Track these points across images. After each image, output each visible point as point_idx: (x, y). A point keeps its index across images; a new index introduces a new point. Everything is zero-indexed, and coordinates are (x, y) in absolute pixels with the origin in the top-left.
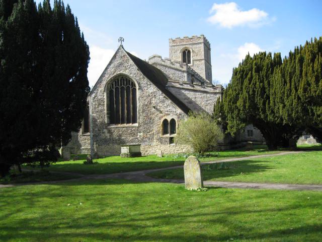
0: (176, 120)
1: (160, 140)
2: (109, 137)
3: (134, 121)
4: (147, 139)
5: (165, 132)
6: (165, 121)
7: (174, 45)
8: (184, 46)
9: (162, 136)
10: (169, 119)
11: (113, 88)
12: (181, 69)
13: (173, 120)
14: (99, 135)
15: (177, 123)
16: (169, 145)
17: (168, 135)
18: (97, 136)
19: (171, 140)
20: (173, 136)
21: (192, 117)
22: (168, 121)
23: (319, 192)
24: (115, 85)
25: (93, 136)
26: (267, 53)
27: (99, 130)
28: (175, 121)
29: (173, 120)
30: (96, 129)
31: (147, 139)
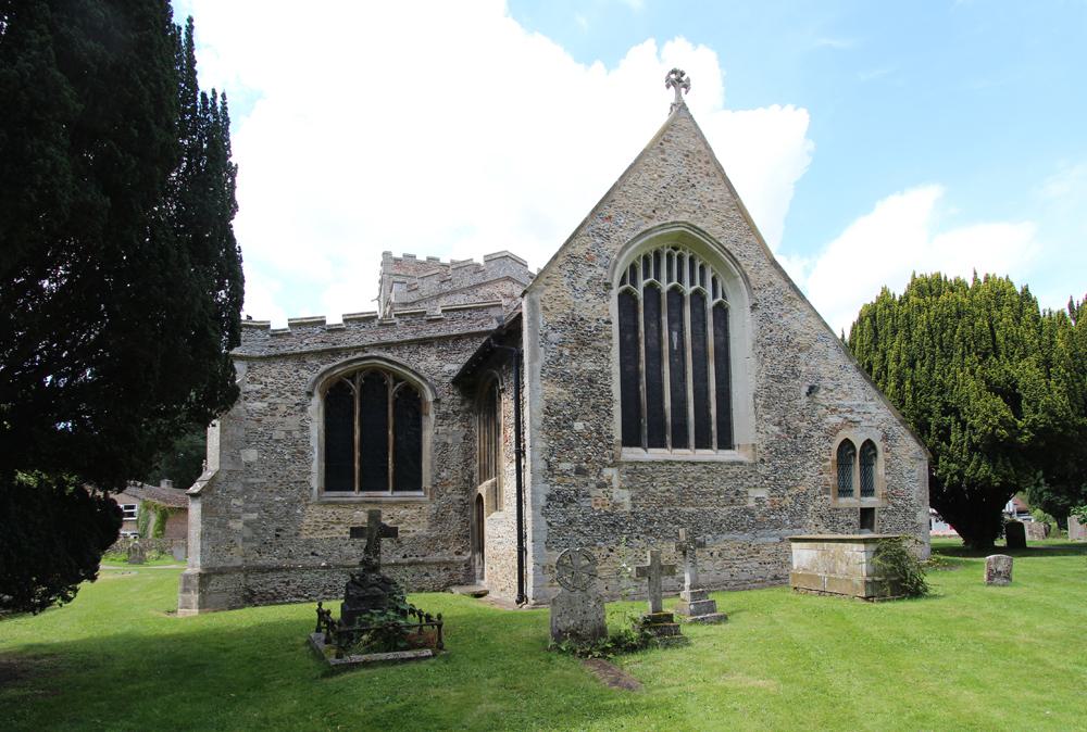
0: (880, 446)
1: (831, 518)
2: (628, 508)
3: (726, 442)
4: (785, 516)
20: (868, 502)
25: (550, 498)
27: (580, 471)
30: (565, 466)
31: (785, 516)
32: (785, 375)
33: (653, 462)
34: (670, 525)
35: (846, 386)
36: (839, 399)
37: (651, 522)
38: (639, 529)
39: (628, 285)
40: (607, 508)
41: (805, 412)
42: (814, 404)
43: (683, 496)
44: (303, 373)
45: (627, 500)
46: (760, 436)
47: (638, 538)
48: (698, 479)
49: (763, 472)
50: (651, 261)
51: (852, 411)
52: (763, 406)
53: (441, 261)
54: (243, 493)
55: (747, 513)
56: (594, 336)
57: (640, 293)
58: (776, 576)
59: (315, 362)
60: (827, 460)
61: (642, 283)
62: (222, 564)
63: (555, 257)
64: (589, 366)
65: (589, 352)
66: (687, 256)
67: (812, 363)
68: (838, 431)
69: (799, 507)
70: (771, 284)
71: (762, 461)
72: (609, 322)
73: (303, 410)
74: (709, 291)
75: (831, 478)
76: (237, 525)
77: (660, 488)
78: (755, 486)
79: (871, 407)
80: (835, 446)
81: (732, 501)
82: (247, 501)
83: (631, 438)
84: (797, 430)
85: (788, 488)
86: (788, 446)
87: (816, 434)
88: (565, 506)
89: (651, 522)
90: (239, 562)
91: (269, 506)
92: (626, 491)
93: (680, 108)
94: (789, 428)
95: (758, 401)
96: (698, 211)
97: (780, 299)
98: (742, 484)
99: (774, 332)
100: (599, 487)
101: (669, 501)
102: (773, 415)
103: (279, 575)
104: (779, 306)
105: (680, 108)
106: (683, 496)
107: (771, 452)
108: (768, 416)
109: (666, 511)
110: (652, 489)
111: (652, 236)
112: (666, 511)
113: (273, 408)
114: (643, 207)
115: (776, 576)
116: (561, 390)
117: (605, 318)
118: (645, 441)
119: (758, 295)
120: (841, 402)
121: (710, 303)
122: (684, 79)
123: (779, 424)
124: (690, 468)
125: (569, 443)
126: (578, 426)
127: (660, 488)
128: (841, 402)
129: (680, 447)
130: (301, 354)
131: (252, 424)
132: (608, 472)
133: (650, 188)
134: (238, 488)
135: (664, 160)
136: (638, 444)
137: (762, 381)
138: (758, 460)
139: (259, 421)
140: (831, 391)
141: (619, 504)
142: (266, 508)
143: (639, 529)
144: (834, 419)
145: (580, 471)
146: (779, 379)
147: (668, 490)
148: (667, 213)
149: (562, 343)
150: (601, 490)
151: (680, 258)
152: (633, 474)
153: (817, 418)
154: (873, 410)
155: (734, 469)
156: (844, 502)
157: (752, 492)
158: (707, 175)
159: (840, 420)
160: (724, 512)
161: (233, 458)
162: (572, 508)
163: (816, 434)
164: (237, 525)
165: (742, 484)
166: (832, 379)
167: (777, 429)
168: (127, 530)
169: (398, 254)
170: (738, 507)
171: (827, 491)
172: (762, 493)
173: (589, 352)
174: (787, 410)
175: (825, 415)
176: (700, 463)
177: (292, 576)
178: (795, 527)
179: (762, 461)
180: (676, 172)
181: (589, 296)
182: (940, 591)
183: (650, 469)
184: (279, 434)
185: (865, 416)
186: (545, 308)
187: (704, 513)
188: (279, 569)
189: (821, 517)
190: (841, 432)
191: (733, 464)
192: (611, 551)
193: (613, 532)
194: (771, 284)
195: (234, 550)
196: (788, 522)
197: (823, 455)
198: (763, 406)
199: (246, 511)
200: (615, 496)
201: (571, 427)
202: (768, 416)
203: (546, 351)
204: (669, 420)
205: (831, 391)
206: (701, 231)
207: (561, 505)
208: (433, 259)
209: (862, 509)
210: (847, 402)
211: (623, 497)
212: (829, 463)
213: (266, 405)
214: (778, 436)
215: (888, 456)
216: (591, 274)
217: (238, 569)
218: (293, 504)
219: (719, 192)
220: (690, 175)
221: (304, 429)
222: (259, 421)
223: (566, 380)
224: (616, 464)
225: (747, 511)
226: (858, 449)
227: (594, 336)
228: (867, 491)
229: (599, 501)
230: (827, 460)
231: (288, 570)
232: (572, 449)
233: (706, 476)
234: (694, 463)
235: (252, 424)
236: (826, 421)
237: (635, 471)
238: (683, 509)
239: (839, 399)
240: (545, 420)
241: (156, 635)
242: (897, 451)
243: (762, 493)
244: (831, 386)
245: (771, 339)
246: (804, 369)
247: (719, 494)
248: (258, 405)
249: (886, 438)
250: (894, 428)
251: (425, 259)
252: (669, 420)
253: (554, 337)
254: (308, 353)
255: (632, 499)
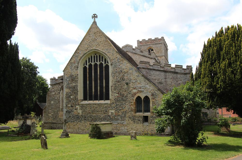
0: (150, 98)
1: (133, 119)
2: (81, 114)
3: (107, 98)
4: (119, 117)
5: (138, 110)
6: (139, 98)
7: (141, 45)
8: (149, 46)
9: (135, 115)
10: (142, 96)
11: (86, 65)
12: (149, 56)
13: (147, 98)
14: (72, 111)
15: (151, 100)
16: (142, 125)
17: (141, 114)
18: (69, 112)
19: (146, 119)
20: (146, 114)
21: (213, 108)
22: (141, 99)
23: (241, 133)
24: (89, 62)
25: (66, 112)
26: (230, 27)
27: (72, 106)
28: (149, 98)
29: (147, 98)
30: (69, 105)
31: (119, 117)
32: (120, 80)
33: (86, 104)
34: (90, 118)
35: (139, 81)
36: (137, 85)
37: (85, 117)
38: (83, 119)
39: (85, 65)
40: (77, 114)
41: (126, 89)
42: (129, 87)
43: (93, 112)
44: (60, 86)
45: (81, 112)
46: (112, 97)
47: (83, 121)
48: (97, 108)
49: (113, 106)
50: (90, 59)
51: (140, 88)
52: (114, 89)
53: (159, 38)
54: (51, 109)
55: (109, 116)
56: (74, 78)
57: (87, 66)
58: (116, 133)
59: (61, 84)
60: (132, 102)
61: (88, 64)
62: (47, 122)
63: (68, 64)
64: (74, 84)
65: (74, 81)
66: (98, 55)
67: (128, 76)
68: (136, 94)
69: (123, 115)
70: (117, 58)
71: (113, 103)
72: (78, 75)
73: (60, 93)
74: (103, 63)
75: (133, 107)
76: (50, 115)
77: (88, 109)
78: (111, 109)
79: (148, 86)
80: (135, 98)
81: (105, 113)
82: (52, 111)
83: (85, 99)
84: (123, 95)
85: (120, 110)
86: (122, 98)
87: (129, 95)
88: (69, 113)
89: (85, 117)
90: (50, 122)
91: (55, 111)
92: (81, 110)
93: (95, 23)
94: (121, 94)
95: (112, 88)
96: (97, 45)
97: (119, 61)
98: (107, 109)
99: (117, 70)
100: (75, 110)
101: (90, 113)
102: (116, 91)
103: (55, 124)
104: (119, 63)
105: (95, 23)
106: (93, 112)
107: (116, 101)
108: (115, 92)
109: (89, 115)
110: (86, 110)
111: (87, 54)
112: (89, 115)
113: (55, 93)
114: (85, 48)
115: (116, 133)
116: (69, 90)
117: (77, 74)
118: (88, 99)
119: (113, 61)
120: (137, 86)
121: (104, 65)
122: (93, 16)
123: (118, 93)
124: (94, 105)
125: (70, 101)
126: (72, 97)
127: (88, 109)
128: (137, 86)
129: (107, 100)
130: (59, 83)
131: (53, 97)
132: (77, 106)
133: (86, 44)
134: (50, 108)
135: (89, 36)
136: (97, 100)
137: (114, 83)
138: (112, 103)
139: (54, 96)
140: (134, 83)
141: (79, 113)
142: (54, 112)
143: (83, 119)
144: (135, 91)
145: (72, 106)
146: (118, 82)
147: (90, 110)
148: (90, 48)
149: (69, 81)
150: (76, 110)
151: (97, 56)
152: (82, 107)
153: (129, 91)
154: (148, 87)
155: (106, 105)
156: (138, 114)
157: (110, 111)
158: (100, 36)
159: (137, 91)
160: (102, 116)
161: (49, 103)
162: (70, 114)
163: (129, 95)
164: (50, 115)
165: (107, 109)
166: (135, 80)
167: (117, 95)
168: (208, 115)
169: (141, 40)
170: (106, 115)
171: (132, 111)
172: (113, 111)
173: (74, 81)
174: (121, 89)
175: (132, 90)
176: (97, 104)
177: (57, 125)
178: (122, 120)
179: (113, 103)
180: (92, 38)
181: (74, 70)
182: (139, 139)
183: (86, 106)
184: (56, 98)
185: (145, 89)
186: (66, 74)
187: (98, 116)
188: (55, 123)
189: (130, 118)
190: (137, 94)
191: (105, 104)
192: (77, 123)
193: (78, 119)
194: (117, 58)
195: (49, 119)
196: (120, 119)
197: (131, 101)
198: (114, 89)
199: (52, 112)
200: (78, 112)
201: (70, 97)
202: (115, 92)
203: (66, 83)
204: (93, 93)
205: (134, 83)
206: (98, 50)
207: (68, 113)
208: (150, 39)
209: (143, 116)
210: (139, 86)
211: (80, 112)
212: (133, 103)
213: (54, 93)
214: (118, 96)
215: (154, 100)
216: (74, 65)
217: (50, 123)
218: (58, 111)
219: (104, 39)
220: (95, 37)
221: (60, 97)
222: (54, 96)
223: (70, 88)
224: (78, 105)
225: (109, 116)
226: (143, 99)
227: (74, 78)
228: (148, 110)
229: (75, 113)
230: (132, 102)
231: (57, 123)
232: (70, 102)
233: (98, 107)
234: (95, 104)
235: (53, 97)
236: (132, 91)
237: (82, 106)
238: (93, 115)
239: (137, 85)
240: (66, 96)
241: (202, 151)
242: (157, 99)
243: (113, 111)
244: (134, 82)
245: (116, 72)
246: (126, 78)
247: (101, 111)
248: (54, 93)
249: (152, 95)
250: (156, 92)
251: (154, 39)
252: (93, 93)
253: (68, 80)
254: (60, 83)
255: (82, 112)
